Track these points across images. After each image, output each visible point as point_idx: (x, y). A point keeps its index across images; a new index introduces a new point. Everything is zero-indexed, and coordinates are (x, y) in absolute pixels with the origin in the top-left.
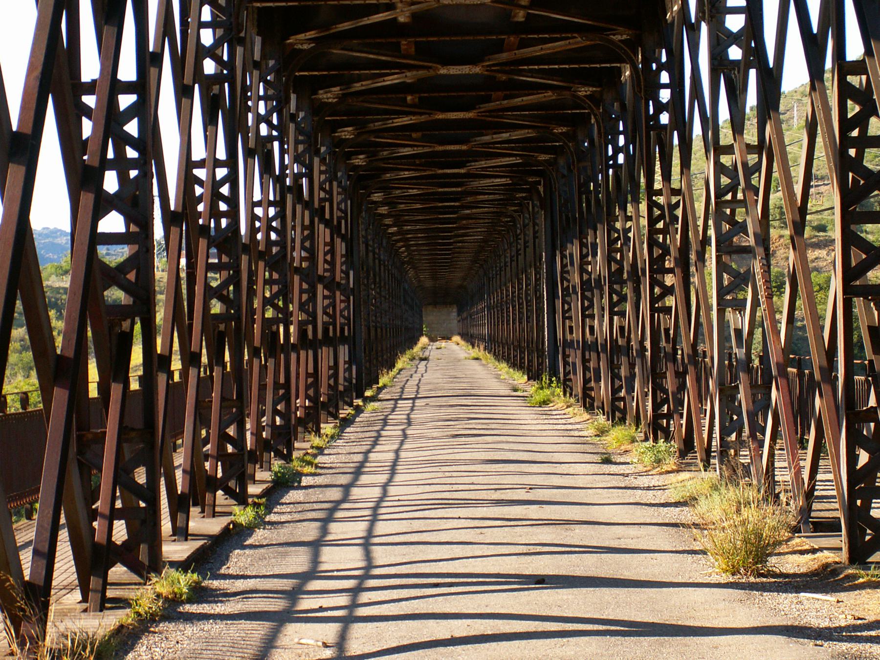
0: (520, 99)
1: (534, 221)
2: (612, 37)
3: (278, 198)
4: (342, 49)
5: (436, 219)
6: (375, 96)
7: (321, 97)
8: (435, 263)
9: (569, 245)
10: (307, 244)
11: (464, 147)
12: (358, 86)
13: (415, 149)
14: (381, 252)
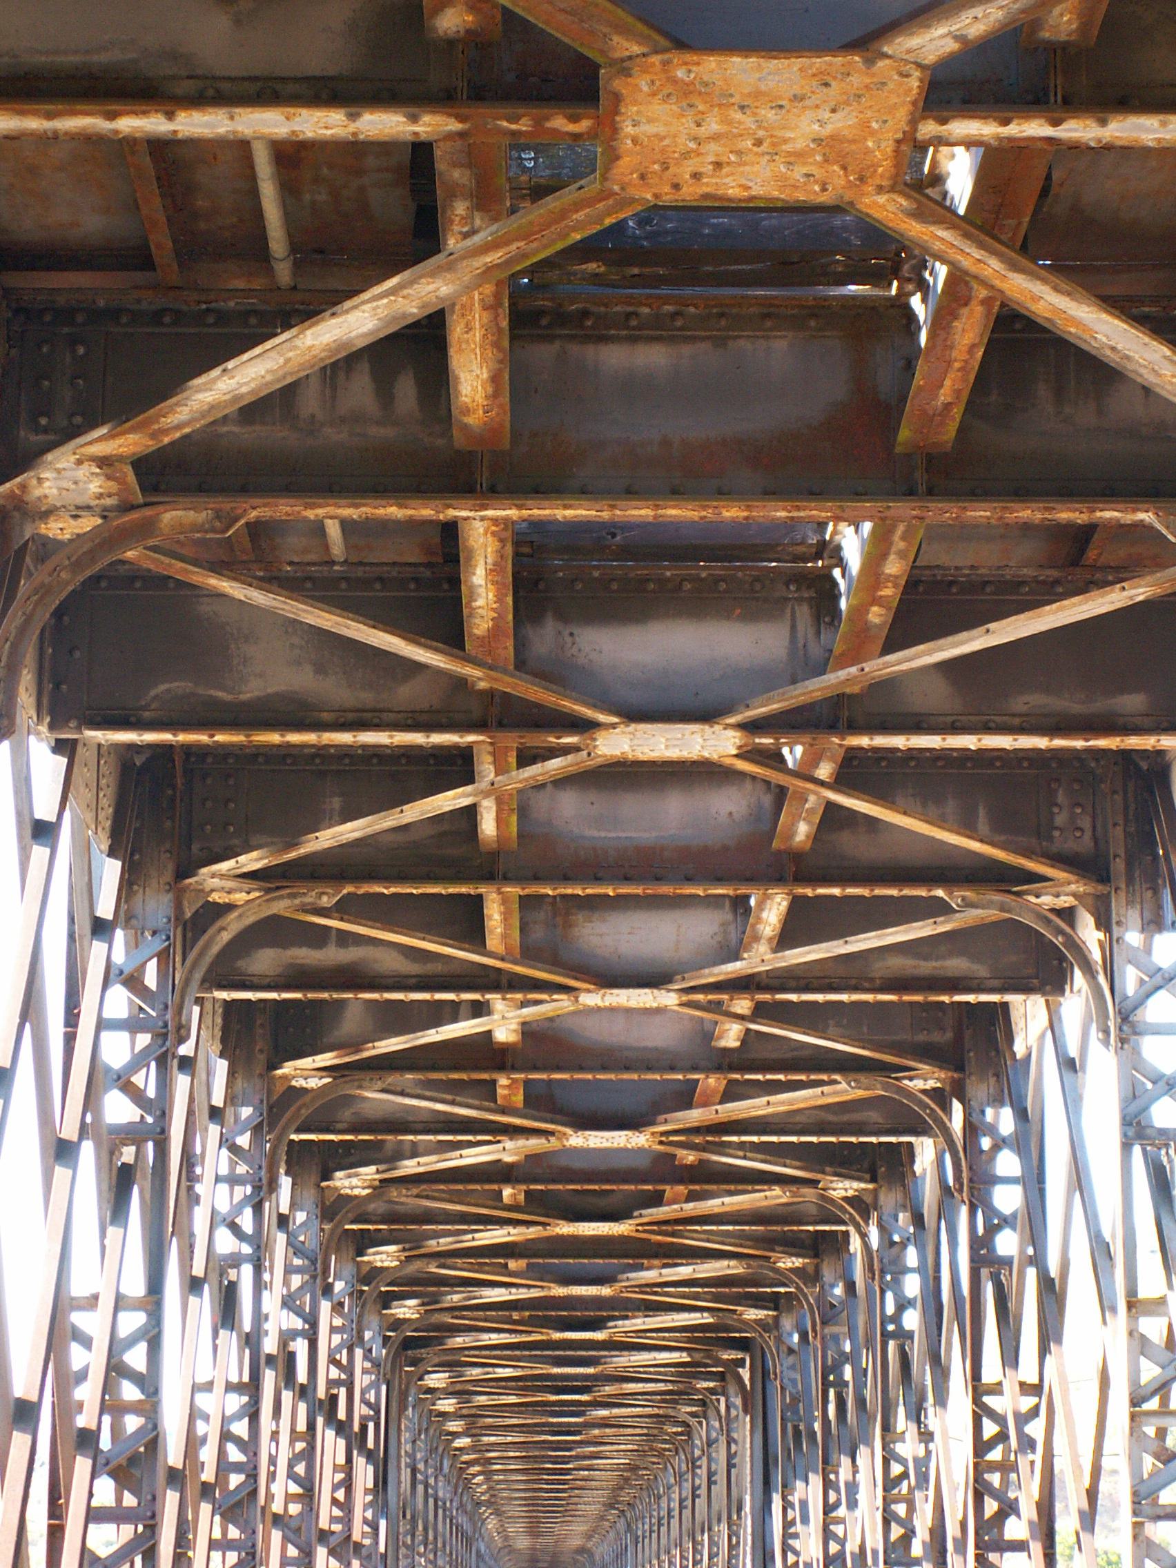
0: (718, 1201)
1: (728, 1435)
2: (906, 1082)
3: (246, 1379)
4: (383, 1091)
5: (543, 1425)
6: (442, 1187)
7: (338, 1184)
8: (538, 1505)
9: (799, 1484)
10: (300, 1469)
11: (606, 1291)
12: (410, 1167)
13: (514, 1290)
14: (440, 1484)
